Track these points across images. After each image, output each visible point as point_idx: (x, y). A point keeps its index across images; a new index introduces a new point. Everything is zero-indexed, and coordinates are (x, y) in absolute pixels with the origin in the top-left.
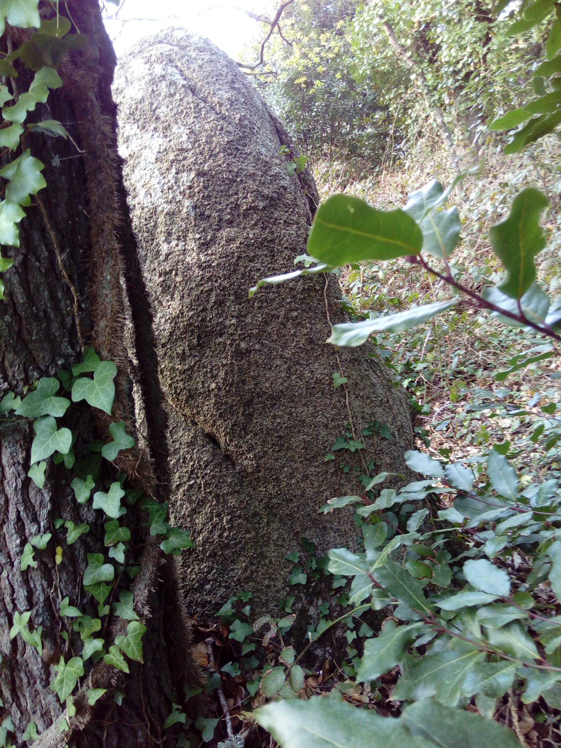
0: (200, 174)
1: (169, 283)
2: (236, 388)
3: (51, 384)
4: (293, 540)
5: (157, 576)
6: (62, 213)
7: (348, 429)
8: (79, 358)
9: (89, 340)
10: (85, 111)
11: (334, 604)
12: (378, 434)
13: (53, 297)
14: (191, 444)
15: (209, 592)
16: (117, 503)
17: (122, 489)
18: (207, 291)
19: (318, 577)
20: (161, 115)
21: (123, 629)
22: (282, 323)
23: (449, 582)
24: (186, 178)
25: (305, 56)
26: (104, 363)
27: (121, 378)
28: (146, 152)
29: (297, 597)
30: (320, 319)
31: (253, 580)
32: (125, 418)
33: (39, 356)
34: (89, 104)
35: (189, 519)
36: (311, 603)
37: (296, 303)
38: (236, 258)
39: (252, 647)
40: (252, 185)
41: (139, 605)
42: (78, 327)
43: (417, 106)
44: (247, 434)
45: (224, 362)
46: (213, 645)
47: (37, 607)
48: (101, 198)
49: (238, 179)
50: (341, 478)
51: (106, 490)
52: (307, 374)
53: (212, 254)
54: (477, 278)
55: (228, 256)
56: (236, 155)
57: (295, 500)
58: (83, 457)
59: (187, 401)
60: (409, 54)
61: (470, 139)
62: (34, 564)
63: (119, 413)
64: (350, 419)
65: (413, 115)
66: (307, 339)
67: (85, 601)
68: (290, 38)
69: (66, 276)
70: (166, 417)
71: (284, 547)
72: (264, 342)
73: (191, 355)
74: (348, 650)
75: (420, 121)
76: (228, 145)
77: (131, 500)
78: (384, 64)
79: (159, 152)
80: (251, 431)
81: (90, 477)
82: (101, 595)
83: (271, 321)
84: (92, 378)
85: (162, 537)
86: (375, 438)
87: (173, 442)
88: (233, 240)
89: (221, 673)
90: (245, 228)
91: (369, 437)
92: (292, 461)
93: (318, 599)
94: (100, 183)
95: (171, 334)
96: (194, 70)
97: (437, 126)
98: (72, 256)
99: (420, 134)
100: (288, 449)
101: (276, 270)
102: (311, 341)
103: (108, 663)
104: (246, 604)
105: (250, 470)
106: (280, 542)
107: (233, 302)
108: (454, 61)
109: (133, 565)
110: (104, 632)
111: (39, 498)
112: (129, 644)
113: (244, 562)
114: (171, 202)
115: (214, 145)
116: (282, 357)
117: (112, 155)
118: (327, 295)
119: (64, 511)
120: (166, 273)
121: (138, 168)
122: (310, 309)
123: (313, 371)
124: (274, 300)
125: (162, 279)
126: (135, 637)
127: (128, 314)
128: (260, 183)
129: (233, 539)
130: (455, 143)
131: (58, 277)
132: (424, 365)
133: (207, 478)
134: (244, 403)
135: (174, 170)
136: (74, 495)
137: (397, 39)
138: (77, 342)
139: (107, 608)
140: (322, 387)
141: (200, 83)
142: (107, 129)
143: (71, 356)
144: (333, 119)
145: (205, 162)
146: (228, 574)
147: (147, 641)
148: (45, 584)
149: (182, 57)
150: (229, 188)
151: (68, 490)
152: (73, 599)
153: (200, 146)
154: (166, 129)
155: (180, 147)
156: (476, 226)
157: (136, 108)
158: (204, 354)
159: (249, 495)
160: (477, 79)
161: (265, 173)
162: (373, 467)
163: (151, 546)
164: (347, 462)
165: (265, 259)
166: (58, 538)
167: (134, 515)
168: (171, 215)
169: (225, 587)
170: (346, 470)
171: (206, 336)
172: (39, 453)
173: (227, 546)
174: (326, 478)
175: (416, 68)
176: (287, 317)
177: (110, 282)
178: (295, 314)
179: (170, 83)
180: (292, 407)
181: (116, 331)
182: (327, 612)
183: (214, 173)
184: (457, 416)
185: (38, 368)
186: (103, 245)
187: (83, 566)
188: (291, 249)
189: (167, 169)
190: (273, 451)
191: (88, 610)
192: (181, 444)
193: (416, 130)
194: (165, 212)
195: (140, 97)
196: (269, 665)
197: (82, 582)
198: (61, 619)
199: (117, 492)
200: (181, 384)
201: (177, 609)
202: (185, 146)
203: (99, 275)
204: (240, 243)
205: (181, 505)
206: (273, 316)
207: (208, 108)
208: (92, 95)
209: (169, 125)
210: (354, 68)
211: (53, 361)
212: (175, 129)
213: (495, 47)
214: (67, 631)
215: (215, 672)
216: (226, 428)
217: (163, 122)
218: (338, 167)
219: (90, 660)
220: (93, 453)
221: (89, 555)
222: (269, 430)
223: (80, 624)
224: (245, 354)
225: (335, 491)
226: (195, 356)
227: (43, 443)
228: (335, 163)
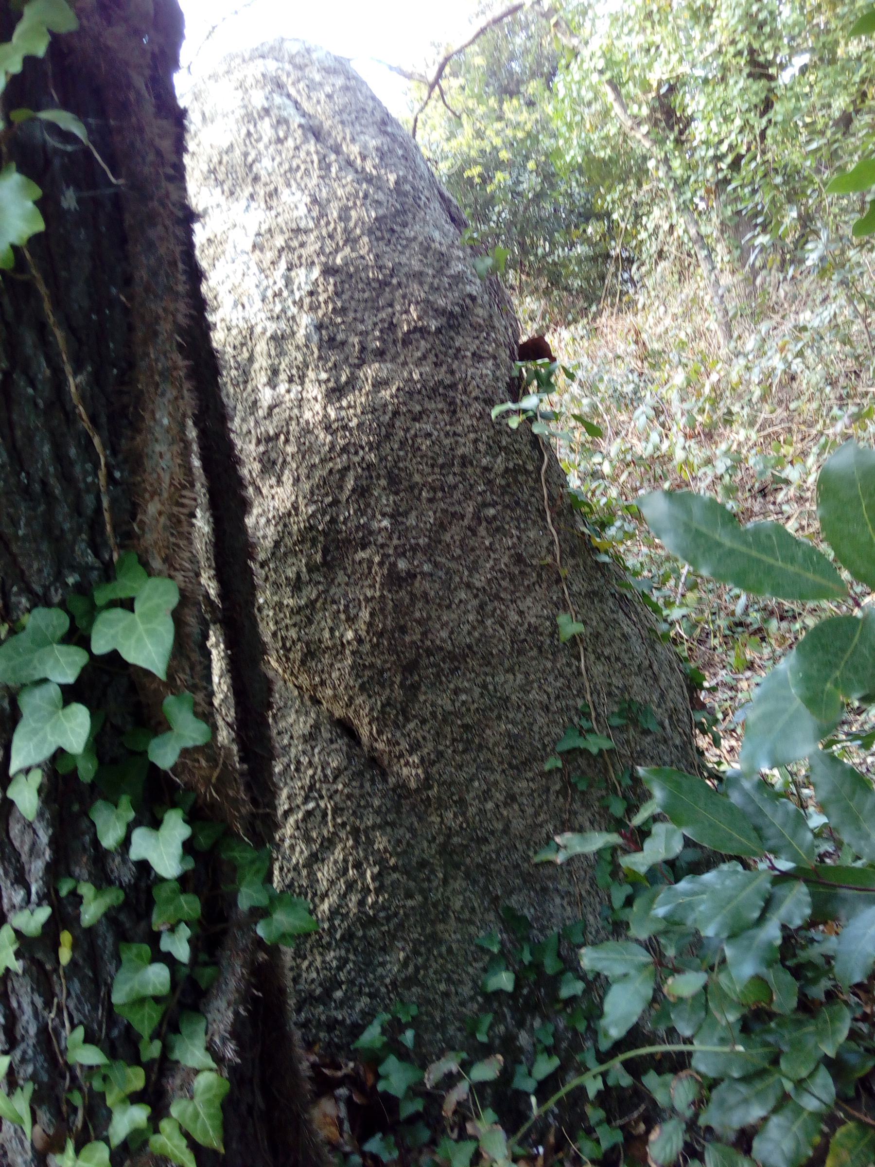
0: (328, 271)
1: (273, 455)
3: (53, 620)
5: (249, 985)
6: (79, 296)
7: (584, 714)
8: (109, 573)
9: (128, 538)
10: (124, 109)
11: (561, 1025)
12: (635, 722)
13: (59, 456)
14: (310, 738)
15: (341, 1004)
16: (177, 849)
17: (185, 821)
18: (339, 471)
19: (532, 977)
20: (263, 174)
21: (187, 1089)
22: (469, 528)
23: (794, 1003)
24: (303, 278)
25: (479, 134)
26: (154, 582)
27: (186, 610)
28: (234, 235)
29: (496, 1013)
30: (534, 523)
31: (418, 983)
32: (194, 688)
33: (31, 566)
34: (132, 96)
35: (304, 872)
36: (521, 1024)
37: (492, 492)
38: (390, 415)
39: (418, 1105)
41: (217, 1040)
42: (107, 516)
43: (656, 211)
44: (407, 720)
45: (369, 594)
46: (349, 1102)
47: (23, 1046)
48: (154, 274)
49: (394, 281)
50: (573, 799)
51: (156, 824)
52: (514, 617)
53: (349, 407)
54: (762, 473)
57: (492, 839)
58: (114, 761)
59: (303, 662)
60: (645, 129)
61: (743, 259)
62: (17, 966)
63: (182, 677)
64: (589, 697)
65: (651, 226)
67: (115, 1033)
68: (458, 106)
69: (84, 416)
70: (268, 685)
72: (438, 559)
74: (589, 1110)
75: (661, 236)
77: (203, 842)
78: (604, 148)
79: (259, 234)
80: (415, 717)
81: (125, 800)
82: (145, 1022)
84: (132, 610)
85: (260, 913)
86: (631, 730)
87: (279, 733)
89: (363, 1154)
90: (405, 364)
91: (621, 729)
92: (486, 769)
93: (533, 1018)
94: (151, 246)
95: (277, 544)
96: (318, 102)
97: (690, 239)
98: (97, 379)
99: (661, 255)
100: (480, 747)
102: (519, 559)
103: (157, 1152)
104: (408, 1026)
105: (413, 785)
106: (466, 915)
108: (716, 139)
109: (206, 964)
110: (150, 1090)
111: (28, 839)
112: (196, 1115)
115: (352, 224)
116: (469, 586)
117: (174, 196)
118: (547, 480)
119: (77, 863)
120: (269, 439)
121: (222, 260)
122: (517, 503)
124: (455, 487)
125: (262, 449)
126: (209, 1103)
127: (201, 490)
129: (384, 908)
130: (719, 266)
131: (70, 417)
132: (684, 611)
133: (337, 798)
134: (403, 666)
135: (283, 265)
136: (95, 834)
137: (625, 107)
138: (105, 544)
139: (157, 1045)
140: (539, 641)
141: (329, 122)
142: (166, 145)
143: (92, 568)
144: (522, 233)
145: (337, 251)
146: (374, 972)
147: (230, 1108)
148: (39, 1001)
149: (299, 81)
151: (84, 824)
152: (93, 1030)
153: (328, 223)
154: (270, 195)
155: (294, 226)
156: (757, 392)
157: (220, 162)
158: (333, 580)
159: (411, 829)
160: (753, 165)
161: (440, 272)
162: (630, 782)
163: (240, 928)
164: (583, 773)
165: (440, 416)
166: (64, 914)
167: (207, 868)
168: (278, 339)
169: (371, 996)
170: (582, 786)
172: (27, 751)
173: (373, 921)
174: (547, 801)
175: (655, 150)
176: (477, 517)
177: (168, 430)
178: (492, 512)
179: (278, 122)
180: (486, 674)
181: (180, 524)
182: (550, 1041)
184: (740, 695)
185: (28, 590)
186: (157, 360)
187: (111, 968)
188: (485, 401)
189: (273, 263)
191: (120, 1050)
192: (292, 737)
193: (654, 249)
194: (268, 334)
195: (225, 145)
196: (449, 1137)
197: (109, 997)
198: (70, 1068)
199: (176, 829)
200: (293, 633)
201: (284, 1039)
202: (302, 225)
203: (147, 416)
204: (398, 389)
205: (292, 847)
206: (454, 515)
207: (343, 163)
208: (139, 82)
209: (276, 189)
210: (558, 153)
211: (59, 577)
212: (285, 194)
213: (779, 118)
214: (80, 1089)
215: (352, 1153)
216: (372, 709)
217: (266, 185)
218: (534, 306)
219: (125, 1145)
220: (133, 753)
221: (123, 946)
222: (446, 715)
223: (105, 1078)
225: (563, 823)
226: (319, 583)
227: (35, 732)
228: (528, 299)
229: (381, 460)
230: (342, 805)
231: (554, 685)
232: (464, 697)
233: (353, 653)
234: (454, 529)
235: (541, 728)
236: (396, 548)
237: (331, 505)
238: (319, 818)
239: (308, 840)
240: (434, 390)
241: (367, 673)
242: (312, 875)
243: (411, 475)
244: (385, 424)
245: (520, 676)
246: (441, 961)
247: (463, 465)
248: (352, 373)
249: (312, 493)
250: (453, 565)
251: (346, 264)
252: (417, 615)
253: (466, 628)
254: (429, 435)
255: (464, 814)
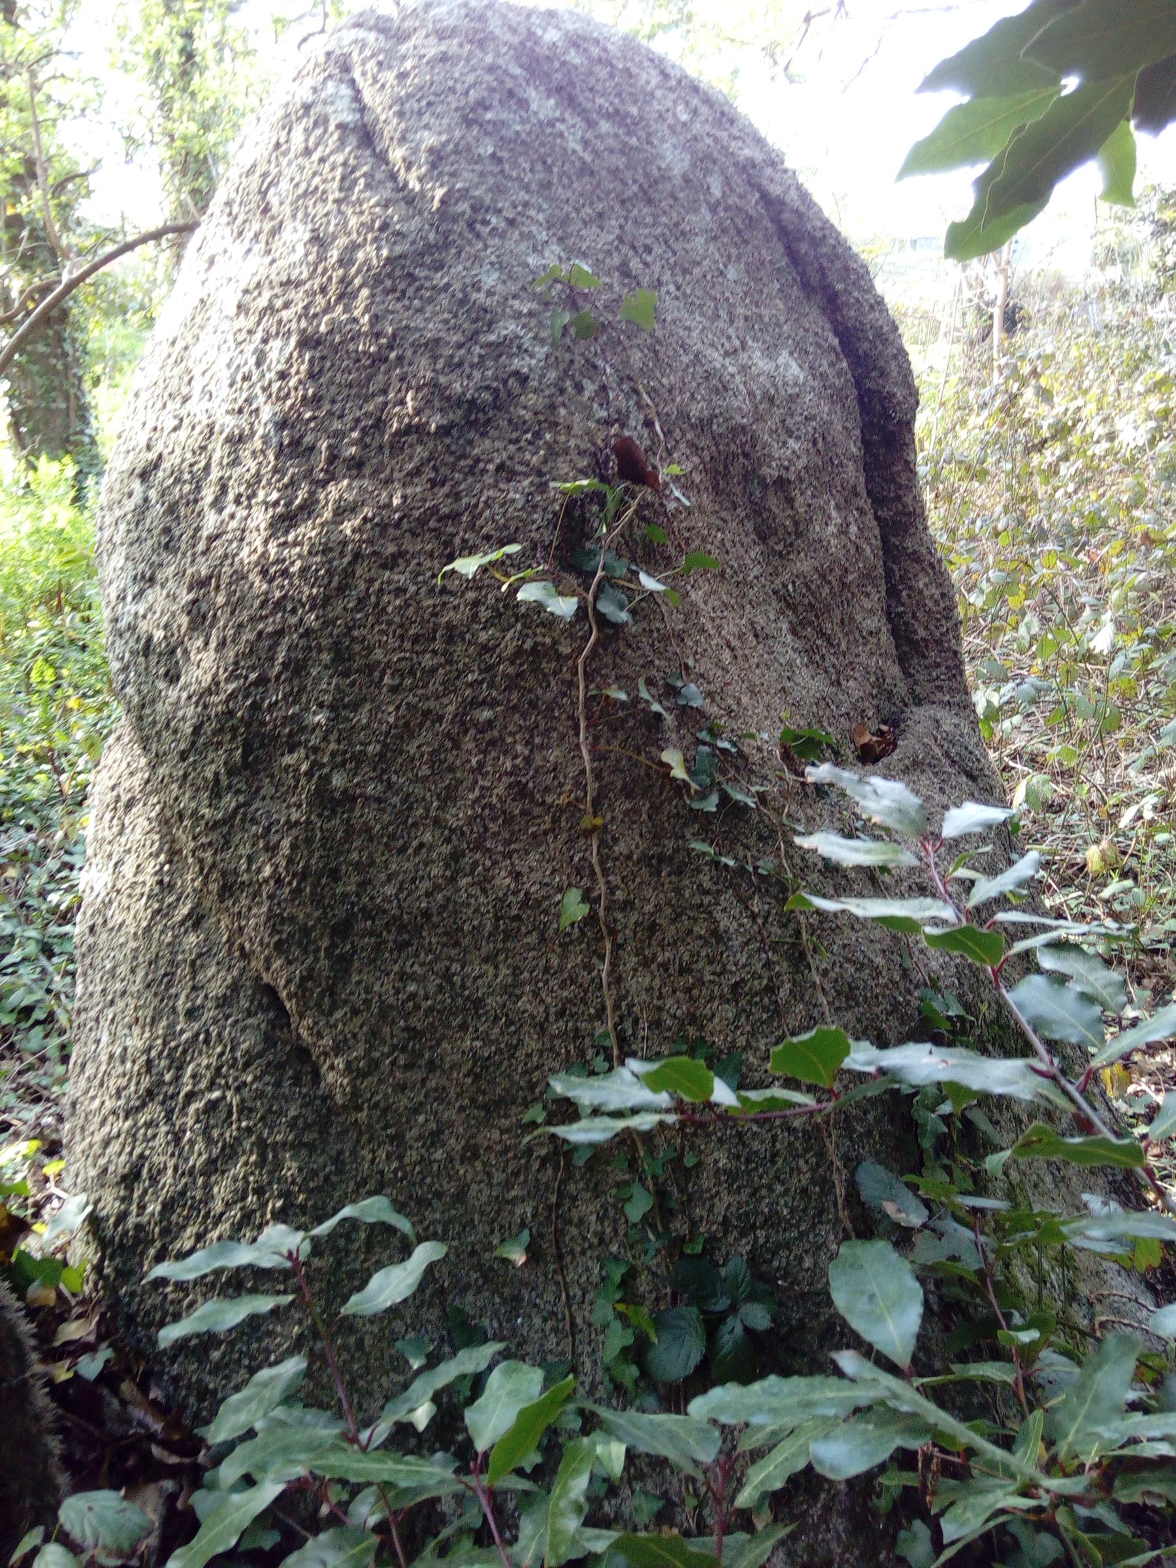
0: (307, 342)
1: (204, 607)
2: (314, 886)
18: (271, 635)
22: (448, 735)
35: (200, 1181)
37: (491, 686)
40: (423, 370)
45: (293, 818)
49: (393, 355)
52: (503, 880)
56: (404, 292)
66: (510, 786)
71: (403, 1318)
73: (230, 787)
76: (388, 269)
80: (346, 1002)
83: (421, 725)
88: (353, 509)
90: (389, 481)
95: (197, 730)
100: (432, 1066)
101: (451, 593)
102: (521, 792)
107: (326, 667)
114: (240, 411)
116: (437, 822)
122: (533, 705)
124: (433, 671)
128: (448, 364)
146: (260, 1340)
150: (369, 379)
159: (337, 1160)
165: (428, 564)
168: (236, 441)
171: (263, 746)
174: (527, 1167)
176: (462, 721)
178: (486, 714)
180: (452, 960)
183: (337, 339)
190: (393, 1063)
204: (365, 520)
205: (192, 1143)
206: (426, 713)
222: (385, 1010)
230: (249, 1104)
231: (556, 994)
232: (412, 988)
234: (424, 736)
235: (529, 1056)
236: (333, 754)
237: (256, 683)
238: (224, 1115)
239: (209, 1141)
240: (422, 522)
241: (287, 929)
242: (207, 1187)
243: (370, 649)
244: (339, 571)
245: (504, 971)
247: (450, 640)
248: (312, 493)
249: (236, 663)
250: (418, 790)
252: (355, 856)
253: (426, 885)
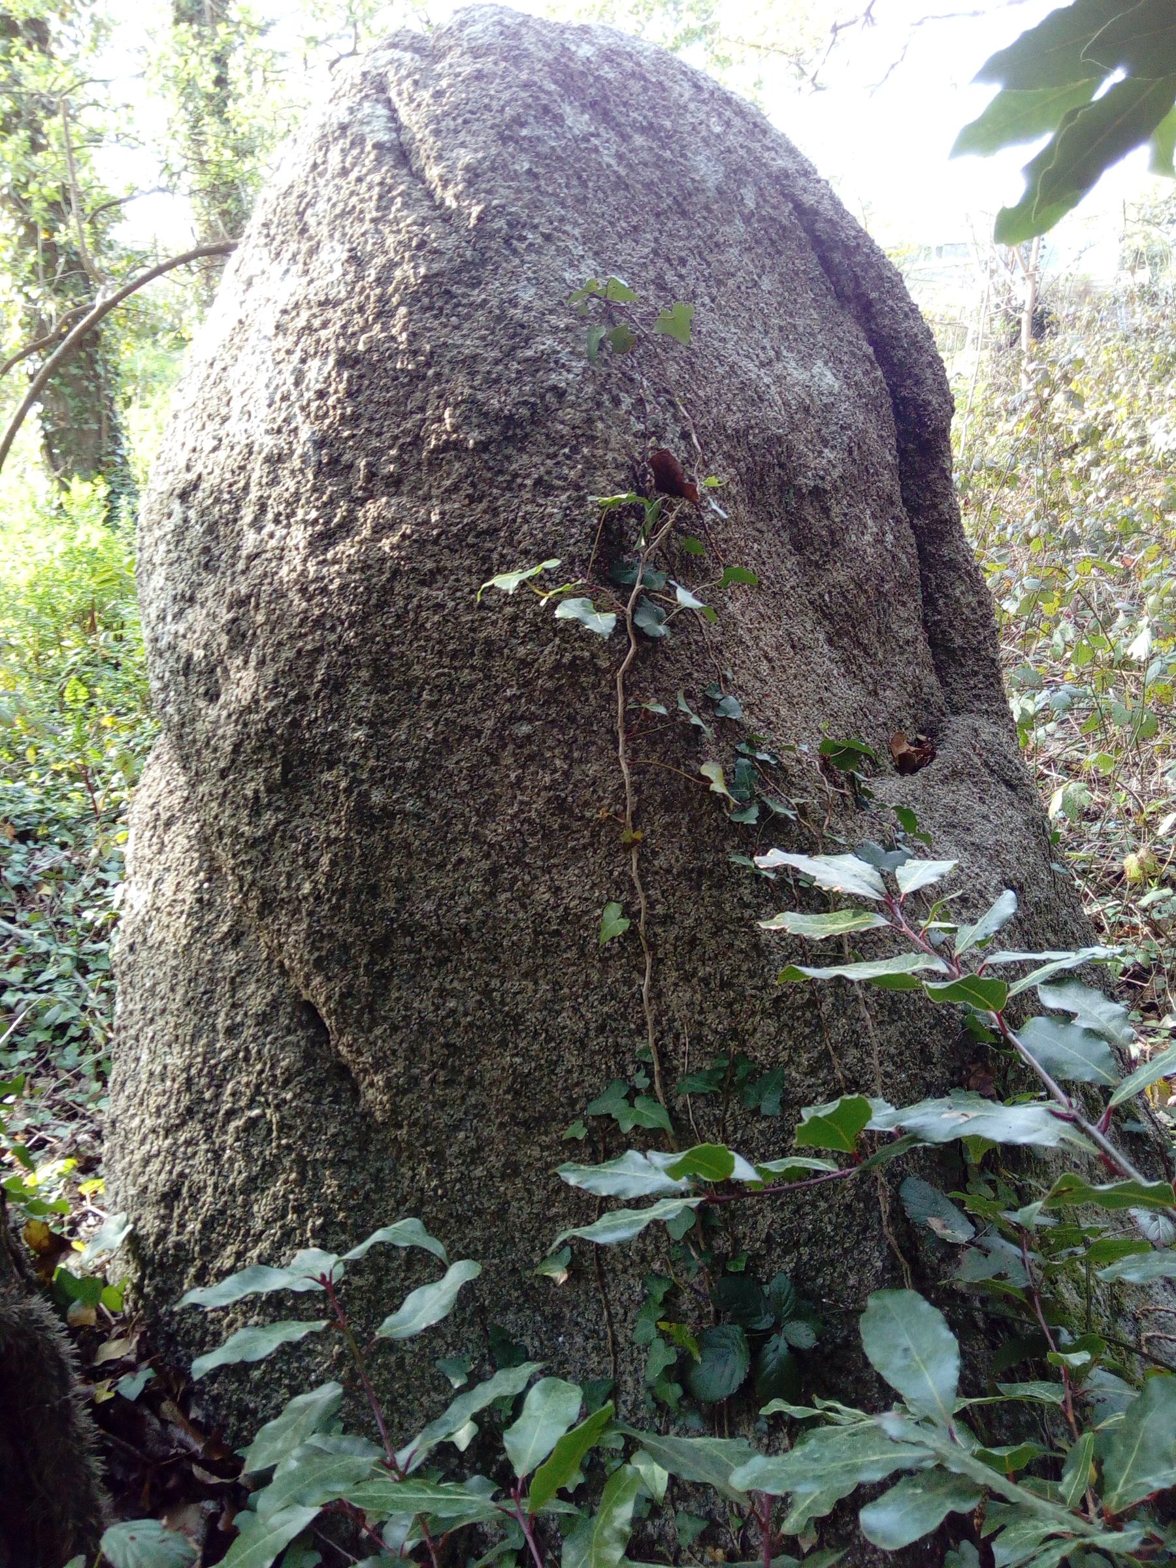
0: (345, 361)
2: (353, 902)
4: (472, 1324)
22: (487, 750)
35: (240, 1199)
44: (374, 1023)
45: (334, 833)
49: (430, 372)
52: (542, 895)
55: (370, 567)
56: (441, 309)
57: (477, 1221)
66: (549, 801)
71: (443, 1337)
73: (269, 804)
76: (426, 286)
80: (385, 1019)
83: (459, 741)
88: (392, 526)
90: (427, 498)
95: (237, 748)
100: (471, 1083)
102: (560, 806)
107: (365, 684)
113: (340, 1341)
116: (476, 838)
122: (571, 719)
123: (558, 889)
128: (486, 380)
146: (300, 1359)
159: (377, 1178)
168: (275, 460)
171: (302, 763)
178: (525, 729)
180: (491, 976)
190: (433, 1080)
204: (404, 536)
206: (465, 729)
222: (424, 1027)
224: (379, 819)
229: (365, 641)
231: (596, 1009)
232: (452, 1004)
233: (310, 914)
235: (569, 1072)
240: (460, 538)
241: (327, 945)
242: (247, 1204)
244: (378, 588)
246: (386, 1375)
247: (488, 655)
248: (350, 511)
250: (458, 806)
251: (369, 351)
252: (394, 872)
254: (440, 606)
255: (440, 1175)
